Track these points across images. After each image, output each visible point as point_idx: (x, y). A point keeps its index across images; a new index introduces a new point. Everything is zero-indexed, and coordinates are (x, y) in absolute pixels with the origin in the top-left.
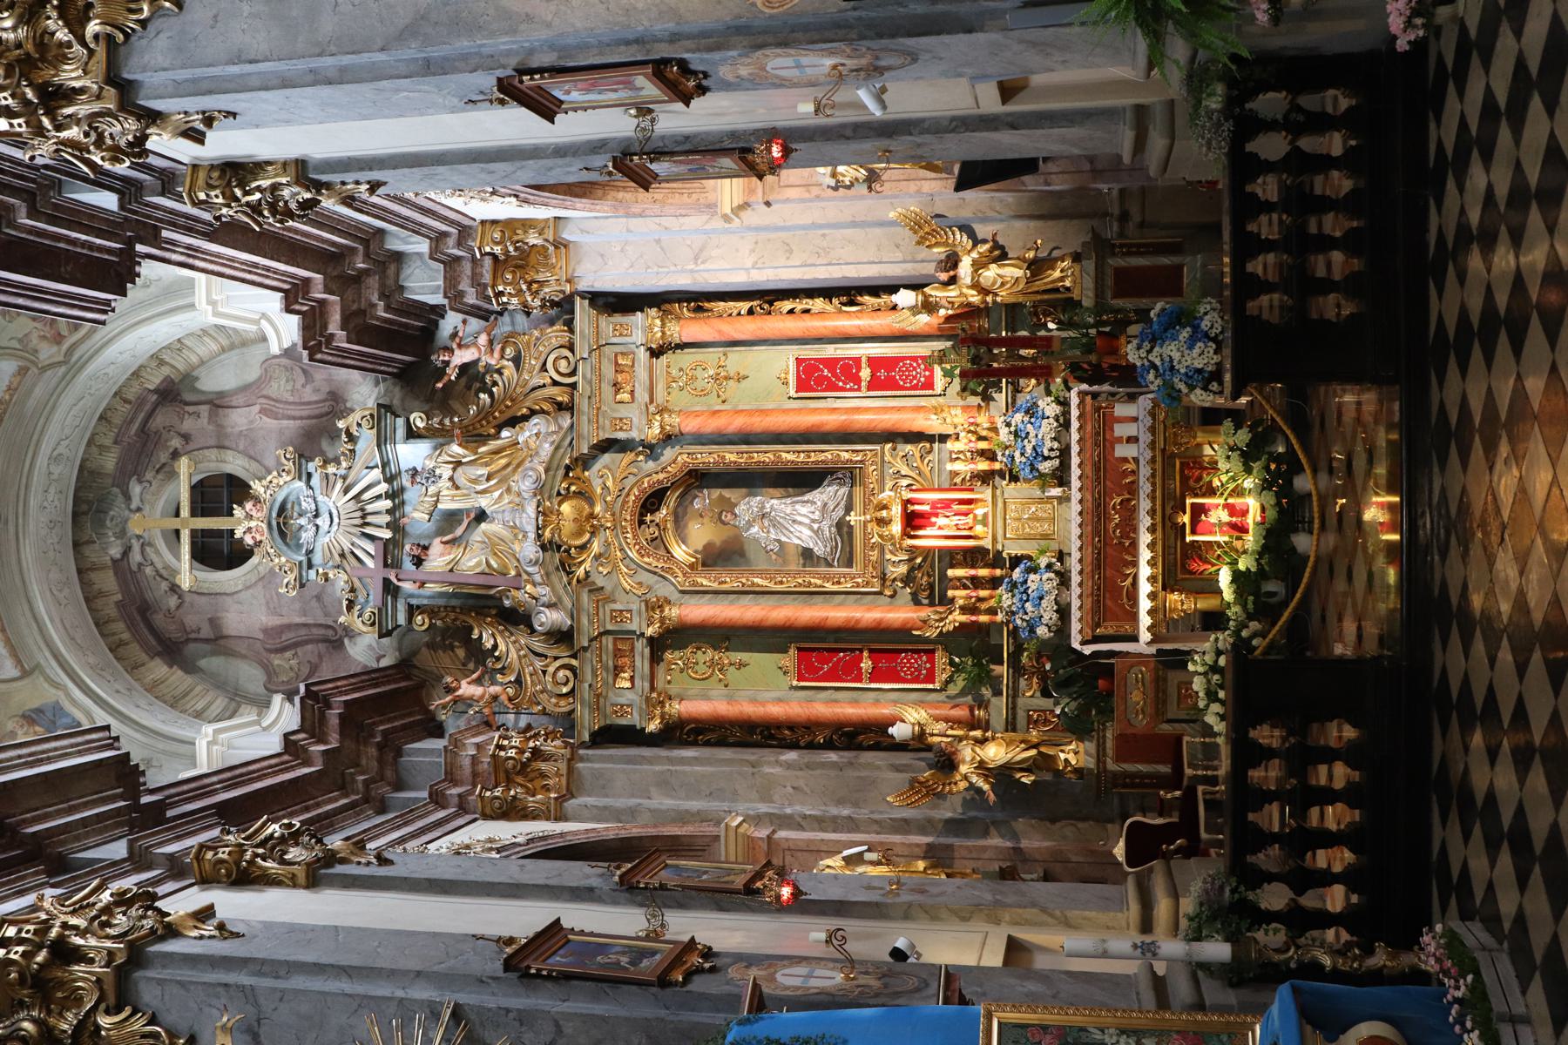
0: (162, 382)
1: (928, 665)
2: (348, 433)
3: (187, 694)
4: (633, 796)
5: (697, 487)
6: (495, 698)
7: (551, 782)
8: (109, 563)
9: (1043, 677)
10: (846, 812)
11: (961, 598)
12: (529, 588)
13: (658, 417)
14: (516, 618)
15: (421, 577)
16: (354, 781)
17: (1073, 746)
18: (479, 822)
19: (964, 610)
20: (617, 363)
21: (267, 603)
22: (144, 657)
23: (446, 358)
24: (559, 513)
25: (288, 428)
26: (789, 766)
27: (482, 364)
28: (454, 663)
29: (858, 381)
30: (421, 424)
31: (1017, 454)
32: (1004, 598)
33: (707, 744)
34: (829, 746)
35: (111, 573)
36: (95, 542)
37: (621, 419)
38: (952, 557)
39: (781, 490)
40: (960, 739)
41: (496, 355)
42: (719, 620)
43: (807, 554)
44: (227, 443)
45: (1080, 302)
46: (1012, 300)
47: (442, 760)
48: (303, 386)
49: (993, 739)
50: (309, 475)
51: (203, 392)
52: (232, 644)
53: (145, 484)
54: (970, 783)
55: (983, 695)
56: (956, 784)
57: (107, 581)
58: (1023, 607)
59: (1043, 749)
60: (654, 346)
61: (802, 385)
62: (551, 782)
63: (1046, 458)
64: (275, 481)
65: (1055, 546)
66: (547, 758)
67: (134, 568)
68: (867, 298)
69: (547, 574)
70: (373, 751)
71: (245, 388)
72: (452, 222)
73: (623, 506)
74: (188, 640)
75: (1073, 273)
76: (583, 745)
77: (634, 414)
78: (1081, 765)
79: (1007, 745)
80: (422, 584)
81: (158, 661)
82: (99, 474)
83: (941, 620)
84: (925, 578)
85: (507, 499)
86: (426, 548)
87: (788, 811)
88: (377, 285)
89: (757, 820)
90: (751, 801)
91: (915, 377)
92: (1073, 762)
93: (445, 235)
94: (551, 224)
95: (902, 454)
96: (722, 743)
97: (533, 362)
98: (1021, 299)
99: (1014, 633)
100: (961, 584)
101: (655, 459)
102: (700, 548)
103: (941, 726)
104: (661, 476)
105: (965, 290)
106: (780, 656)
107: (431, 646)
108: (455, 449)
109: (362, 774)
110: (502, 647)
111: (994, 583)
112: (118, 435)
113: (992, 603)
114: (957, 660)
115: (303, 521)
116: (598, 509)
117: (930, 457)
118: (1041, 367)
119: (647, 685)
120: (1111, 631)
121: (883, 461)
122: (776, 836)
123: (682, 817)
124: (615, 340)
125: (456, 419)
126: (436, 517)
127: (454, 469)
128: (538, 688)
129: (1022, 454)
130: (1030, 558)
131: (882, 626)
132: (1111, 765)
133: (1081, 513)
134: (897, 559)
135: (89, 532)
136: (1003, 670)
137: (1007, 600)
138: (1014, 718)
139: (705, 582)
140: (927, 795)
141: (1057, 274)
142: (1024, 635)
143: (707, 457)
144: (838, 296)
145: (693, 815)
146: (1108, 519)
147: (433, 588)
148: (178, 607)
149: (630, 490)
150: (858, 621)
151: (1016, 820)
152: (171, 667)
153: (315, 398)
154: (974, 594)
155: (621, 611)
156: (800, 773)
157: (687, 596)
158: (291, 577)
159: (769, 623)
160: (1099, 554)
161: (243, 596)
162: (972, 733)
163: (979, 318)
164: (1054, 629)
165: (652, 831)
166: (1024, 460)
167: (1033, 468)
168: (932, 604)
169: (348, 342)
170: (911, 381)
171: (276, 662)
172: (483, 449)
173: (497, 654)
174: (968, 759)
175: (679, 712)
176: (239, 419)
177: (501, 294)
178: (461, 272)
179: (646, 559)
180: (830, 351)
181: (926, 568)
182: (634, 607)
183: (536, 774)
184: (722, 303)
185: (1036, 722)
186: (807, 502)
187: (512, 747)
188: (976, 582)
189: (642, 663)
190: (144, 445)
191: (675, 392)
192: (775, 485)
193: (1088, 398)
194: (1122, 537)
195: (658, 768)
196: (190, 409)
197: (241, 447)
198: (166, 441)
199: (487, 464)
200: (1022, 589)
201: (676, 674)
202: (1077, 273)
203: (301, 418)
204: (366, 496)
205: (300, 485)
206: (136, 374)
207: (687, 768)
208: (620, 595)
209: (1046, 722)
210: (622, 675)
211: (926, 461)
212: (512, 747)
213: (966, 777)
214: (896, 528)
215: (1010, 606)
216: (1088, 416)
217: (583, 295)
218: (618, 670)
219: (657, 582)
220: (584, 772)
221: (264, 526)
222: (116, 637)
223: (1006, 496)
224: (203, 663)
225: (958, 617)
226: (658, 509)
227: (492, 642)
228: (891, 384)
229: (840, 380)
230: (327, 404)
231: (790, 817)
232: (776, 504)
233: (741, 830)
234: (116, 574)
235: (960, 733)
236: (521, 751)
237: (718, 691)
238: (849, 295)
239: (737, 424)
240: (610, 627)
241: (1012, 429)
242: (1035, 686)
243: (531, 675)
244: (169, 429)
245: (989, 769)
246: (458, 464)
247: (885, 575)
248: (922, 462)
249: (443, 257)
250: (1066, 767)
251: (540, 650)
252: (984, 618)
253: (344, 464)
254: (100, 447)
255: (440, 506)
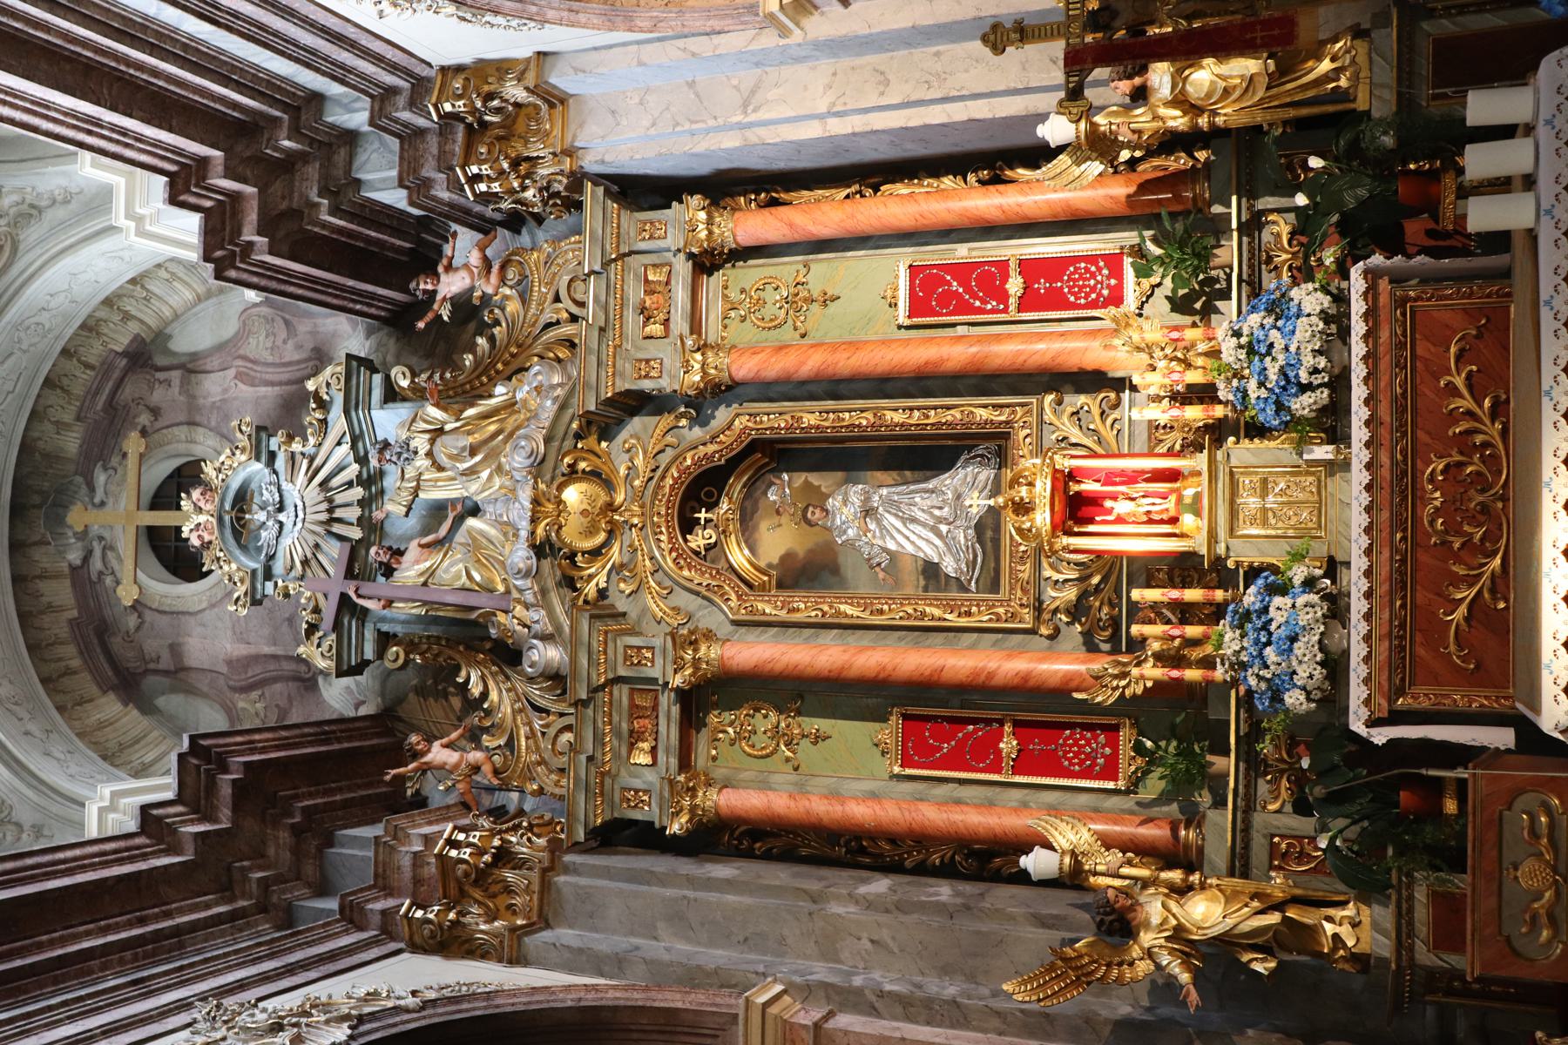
0: (132, 341)
1: (1108, 751)
2: (316, 394)
3: (137, 742)
4: (632, 933)
5: (771, 471)
6: (476, 769)
7: (518, 901)
8: (67, 570)
9: (1300, 780)
10: (951, 990)
11: (1157, 638)
12: (519, 610)
13: (698, 356)
14: (508, 655)
15: (389, 593)
16: (246, 879)
17: (1350, 911)
18: (405, 956)
19: (1161, 658)
20: (647, 281)
21: (234, 626)
22: (94, 690)
23: (429, 287)
24: (560, 502)
25: (265, 397)
26: (869, 904)
27: (477, 294)
28: (448, 718)
29: (1003, 297)
30: (405, 383)
31: (1252, 385)
32: (1227, 638)
33: (767, 857)
34: (947, 871)
35: (67, 582)
36: (49, 544)
37: (647, 361)
38: (1148, 570)
39: (894, 474)
40: (1146, 884)
41: (494, 278)
42: (779, 667)
43: (931, 571)
44: (198, 419)
45: (1368, 113)
46: (1243, 120)
47: (371, 854)
48: (285, 342)
49: (1203, 887)
50: (272, 456)
51: (174, 354)
52: (193, 678)
53: (111, 472)
54: (1158, 967)
55: (1196, 804)
56: (1131, 964)
57: (60, 593)
58: (1261, 655)
59: (1291, 914)
60: (695, 250)
61: (917, 306)
62: (518, 901)
63: (1304, 388)
64: (228, 462)
65: (1321, 550)
66: (519, 864)
67: (94, 577)
68: (1020, 171)
69: (544, 592)
70: (284, 836)
71: (220, 347)
72: (394, 68)
73: (655, 494)
74: (147, 672)
75: (1353, 61)
76: (576, 847)
77: (665, 352)
78: (1364, 947)
79: (1227, 901)
80: (389, 603)
81: (111, 696)
82: (58, 457)
83: (1124, 675)
84: (1105, 610)
85: (497, 482)
86: (400, 553)
87: (858, 981)
88: (316, 176)
89: (806, 992)
90: (806, 957)
91: (1093, 289)
92: (1350, 943)
93: (392, 91)
94: (532, 65)
95: (1070, 410)
96: (788, 856)
97: (543, 290)
98: (1259, 118)
99: (1247, 700)
100: (1156, 612)
101: (703, 424)
102: (775, 561)
103: (1115, 857)
104: (711, 448)
105: (1163, 111)
106: (877, 726)
107: (421, 691)
108: (433, 412)
109: (261, 868)
110: (494, 695)
111: (1216, 613)
112: (81, 409)
113: (1209, 649)
114: (1149, 744)
115: (261, 516)
116: (619, 498)
117: (1116, 414)
118: (1268, 24)
119: (674, 762)
120: (1425, 704)
121: (1041, 422)
122: (831, 1024)
123: (693, 977)
124: (643, 246)
125: (448, 375)
126: (417, 509)
127: (432, 441)
128: (534, 757)
129: (1261, 384)
130: (1275, 570)
131: (1031, 683)
132: (1424, 955)
133: (1369, 488)
134: (1061, 577)
135: (42, 530)
136: (1227, 764)
137: (1231, 641)
138: (1247, 846)
139: (767, 608)
140: (1077, 983)
141: (1326, 66)
142: (1261, 704)
143: (774, 419)
144: (975, 171)
145: (708, 974)
146: (1420, 498)
147: (403, 609)
148: (138, 628)
149: (667, 470)
150: (991, 675)
151: (1242, 1033)
152: (126, 705)
153: (296, 357)
154: (1176, 632)
155: (639, 648)
156: (883, 918)
157: (743, 630)
158: (241, 590)
159: (853, 672)
160: (1403, 561)
161: (208, 615)
162: (1165, 875)
163: (1194, 182)
164: (1317, 695)
165: (638, 998)
166: (1263, 393)
167: (1280, 407)
168: (1115, 650)
169: (271, 253)
170: (1087, 295)
171: (241, 704)
172: (470, 412)
173: (485, 706)
174: (1155, 920)
175: (716, 806)
176: (214, 386)
177: (477, 178)
178: (425, 150)
179: (686, 573)
180: (962, 252)
181: (1108, 590)
182: (657, 642)
183: (500, 886)
184: (805, 193)
185: (1285, 855)
186: (933, 492)
187: (469, 845)
188: (1185, 612)
189: (669, 731)
190: (112, 422)
191: (734, 325)
192: (885, 467)
193: (1384, 285)
194: (1446, 532)
195: (669, 892)
196: (161, 375)
197: (213, 424)
198: (134, 418)
199: (469, 433)
200: (1259, 624)
201: (724, 747)
202: (1362, 59)
203: (280, 384)
204: (335, 482)
205: (258, 467)
206: (89, 327)
207: (713, 896)
208: (649, 626)
209: (1303, 857)
210: (641, 745)
211: (1109, 421)
212: (469, 845)
213: (1149, 954)
214: (1042, 518)
215: (1237, 653)
216: (1384, 314)
217: (598, 179)
218: (634, 738)
219: (700, 607)
220: (566, 890)
221: (214, 521)
222: (64, 664)
223: (1234, 462)
224: (161, 702)
225: (1152, 672)
226: (716, 504)
227: (480, 688)
228: (1056, 301)
229: (976, 297)
230: (311, 364)
231: (859, 992)
232: (884, 490)
233: (774, 1010)
234: (74, 585)
235: (1144, 873)
236: (480, 852)
237: (784, 777)
238: (991, 167)
239: (811, 363)
240: (622, 672)
241: (1244, 340)
242: (1284, 794)
243: (527, 738)
244: (138, 401)
245: (1192, 942)
246: (439, 432)
247: (1041, 603)
248: (1103, 421)
249: (396, 127)
250: (1334, 949)
251: (542, 703)
252: (1192, 674)
253: (312, 441)
254: (57, 423)
255: (422, 495)
